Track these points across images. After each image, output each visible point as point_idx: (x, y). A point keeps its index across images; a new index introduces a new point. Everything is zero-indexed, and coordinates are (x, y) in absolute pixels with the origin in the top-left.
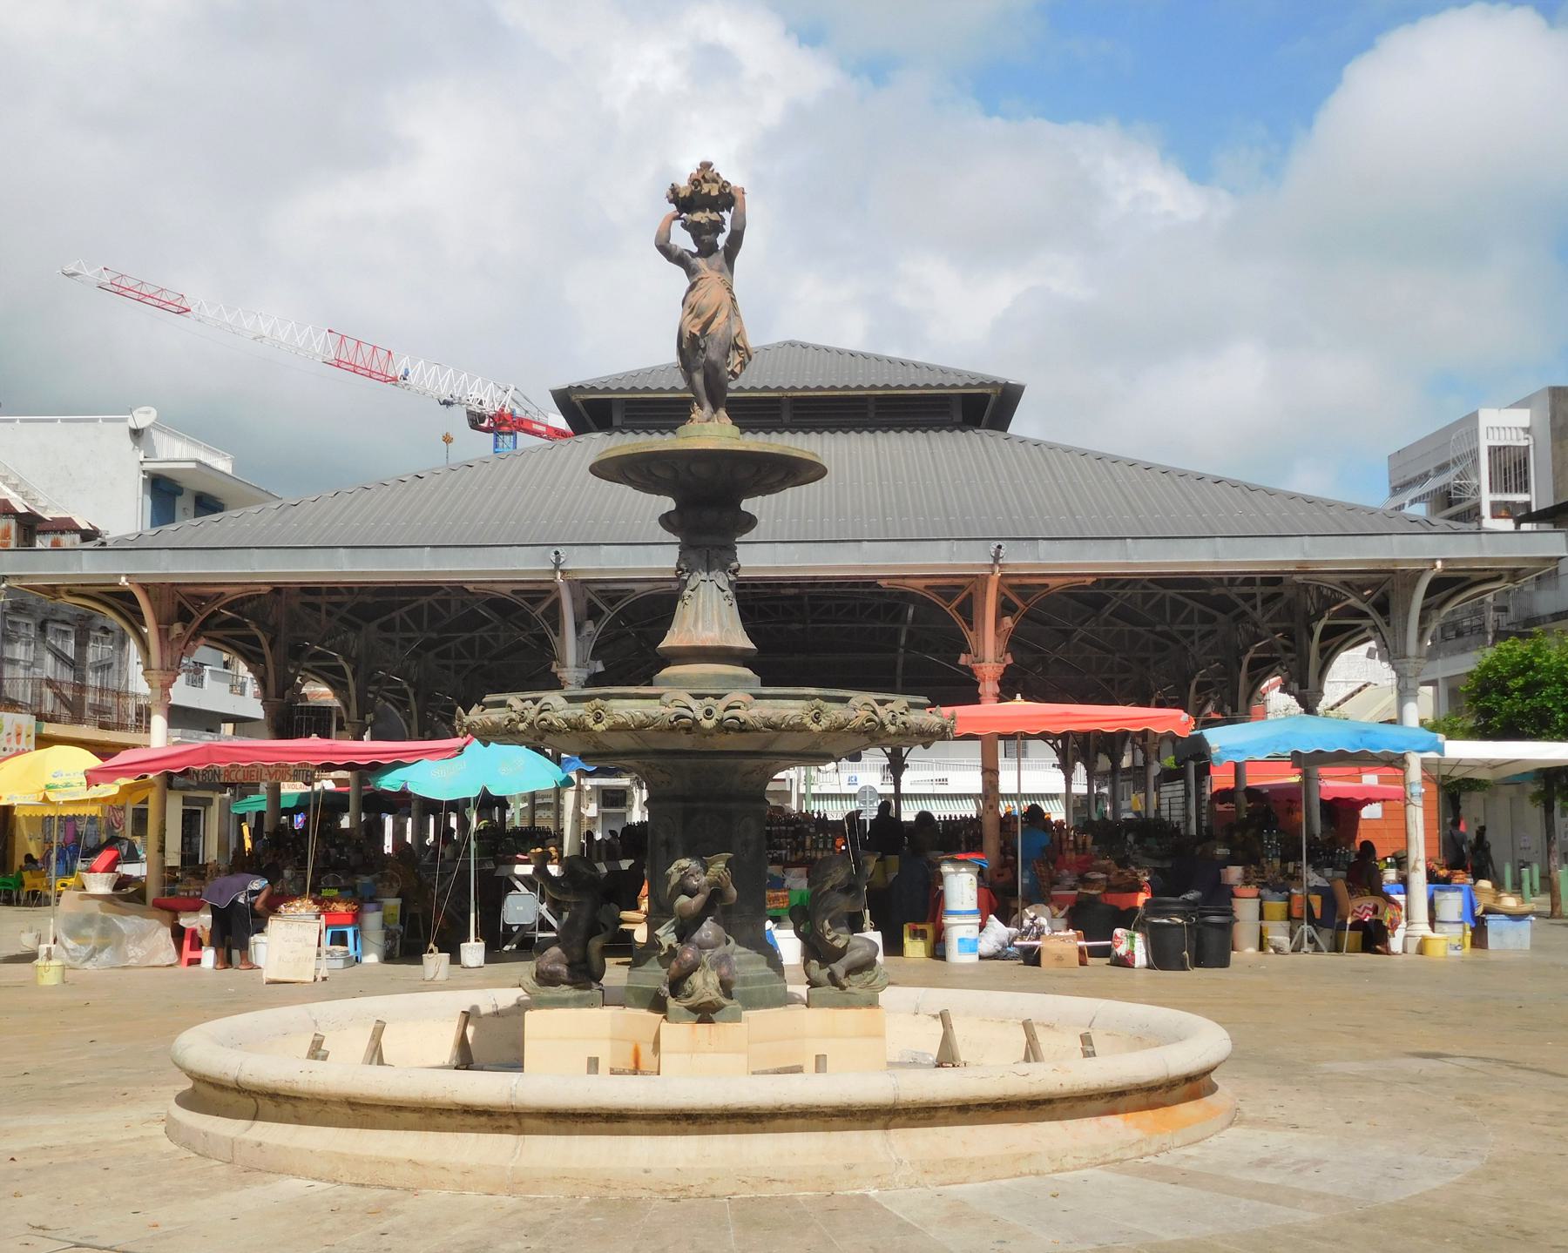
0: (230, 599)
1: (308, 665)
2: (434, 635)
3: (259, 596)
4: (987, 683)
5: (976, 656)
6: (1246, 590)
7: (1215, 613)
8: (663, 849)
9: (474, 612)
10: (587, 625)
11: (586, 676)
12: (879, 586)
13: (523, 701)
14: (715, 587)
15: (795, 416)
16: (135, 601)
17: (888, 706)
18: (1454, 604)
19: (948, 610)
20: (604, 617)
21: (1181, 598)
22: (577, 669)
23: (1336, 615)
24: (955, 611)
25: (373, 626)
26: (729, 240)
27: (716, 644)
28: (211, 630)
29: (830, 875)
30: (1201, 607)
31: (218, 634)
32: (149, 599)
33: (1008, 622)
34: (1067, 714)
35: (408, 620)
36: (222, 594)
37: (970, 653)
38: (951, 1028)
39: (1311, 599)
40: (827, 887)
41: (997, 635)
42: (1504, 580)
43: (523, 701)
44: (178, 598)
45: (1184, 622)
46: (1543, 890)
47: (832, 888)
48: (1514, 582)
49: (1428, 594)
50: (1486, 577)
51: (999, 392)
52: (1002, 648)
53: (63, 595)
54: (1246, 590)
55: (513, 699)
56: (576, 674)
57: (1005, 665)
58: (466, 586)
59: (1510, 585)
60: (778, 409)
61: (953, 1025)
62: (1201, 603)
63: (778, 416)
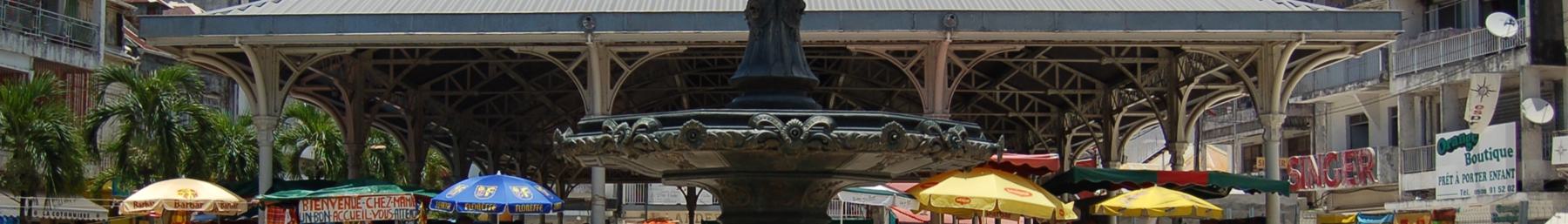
0: (321, 58)
1: (378, 117)
2: (476, 94)
3: (341, 57)
6: (1129, 60)
7: (1094, 80)
9: (505, 75)
12: (848, 52)
16: (247, 62)
17: (950, 130)
18: (1314, 66)
19: (904, 70)
20: (624, 74)
21: (1067, 68)
23: (1130, 110)
25: (427, 86)
28: (303, 86)
30: (1083, 75)
31: (310, 89)
32: (257, 57)
35: (455, 81)
36: (315, 55)
39: (1181, 68)
42: (1349, 52)
44: (280, 58)
45: (1070, 87)
46: (1383, 206)
48: (1356, 54)
49: (1292, 59)
50: (1332, 50)
53: (189, 55)
54: (1129, 60)
58: (512, 48)
59: (1352, 56)
62: (1084, 73)
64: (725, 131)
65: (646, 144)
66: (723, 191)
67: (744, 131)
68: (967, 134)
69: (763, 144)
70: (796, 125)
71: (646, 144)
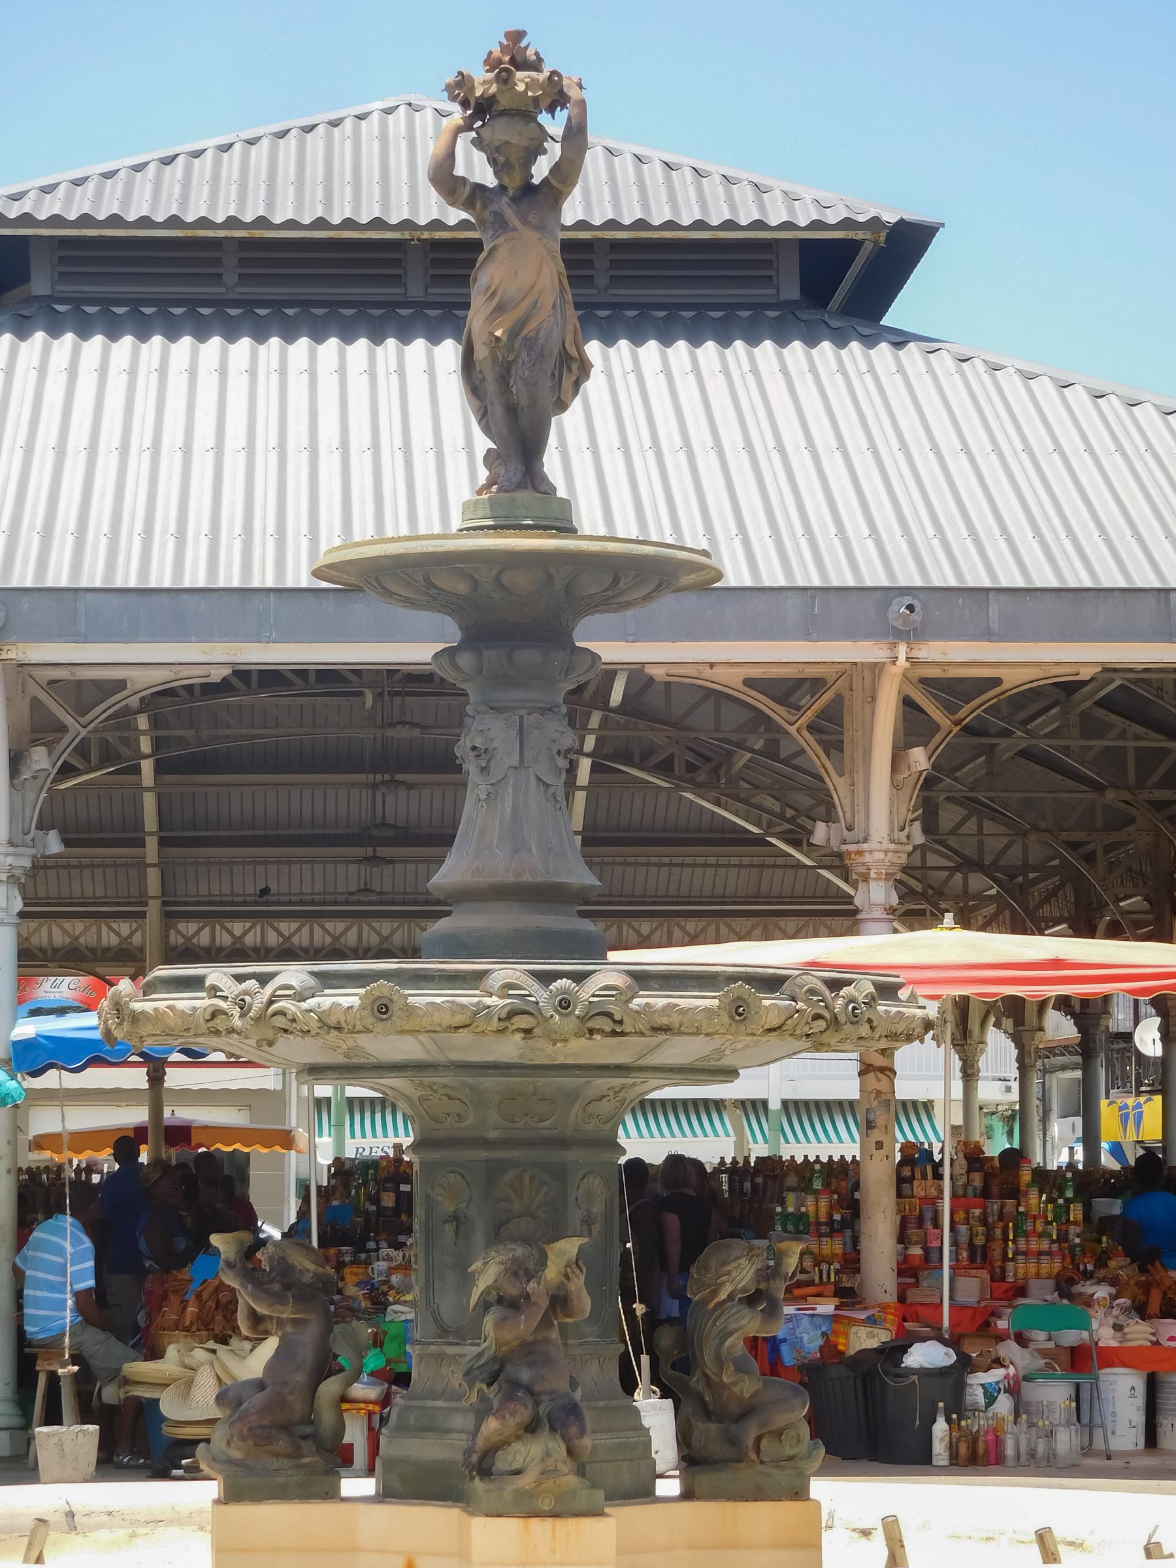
4: (873, 885)
5: (850, 828)
8: (449, 1228)
10: (35, 757)
11: (27, 863)
13: (240, 978)
14: (533, 781)
15: (437, 280)
17: (845, 991)
19: (792, 730)
22: (11, 849)
24: (806, 733)
26: (556, 169)
27: (540, 879)
29: (729, 1273)
33: (919, 758)
34: (1057, 964)
37: (837, 821)
38: (903, 1546)
40: (723, 1295)
41: (895, 786)
43: (240, 978)
47: (730, 1297)
51: (883, 239)
52: (903, 813)
55: (217, 975)
56: (9, 860)
57: (910, 848)
60: (397, 263)
61: (905, 1543)
63: (397, 279)
64: (439, 1000)
65: (294, 1020)
66: (422, 1099)
67: (476, 999)
68: (876, 995)
69: (507, 1024)
70: (564, 991)
71: (294, 1020)
